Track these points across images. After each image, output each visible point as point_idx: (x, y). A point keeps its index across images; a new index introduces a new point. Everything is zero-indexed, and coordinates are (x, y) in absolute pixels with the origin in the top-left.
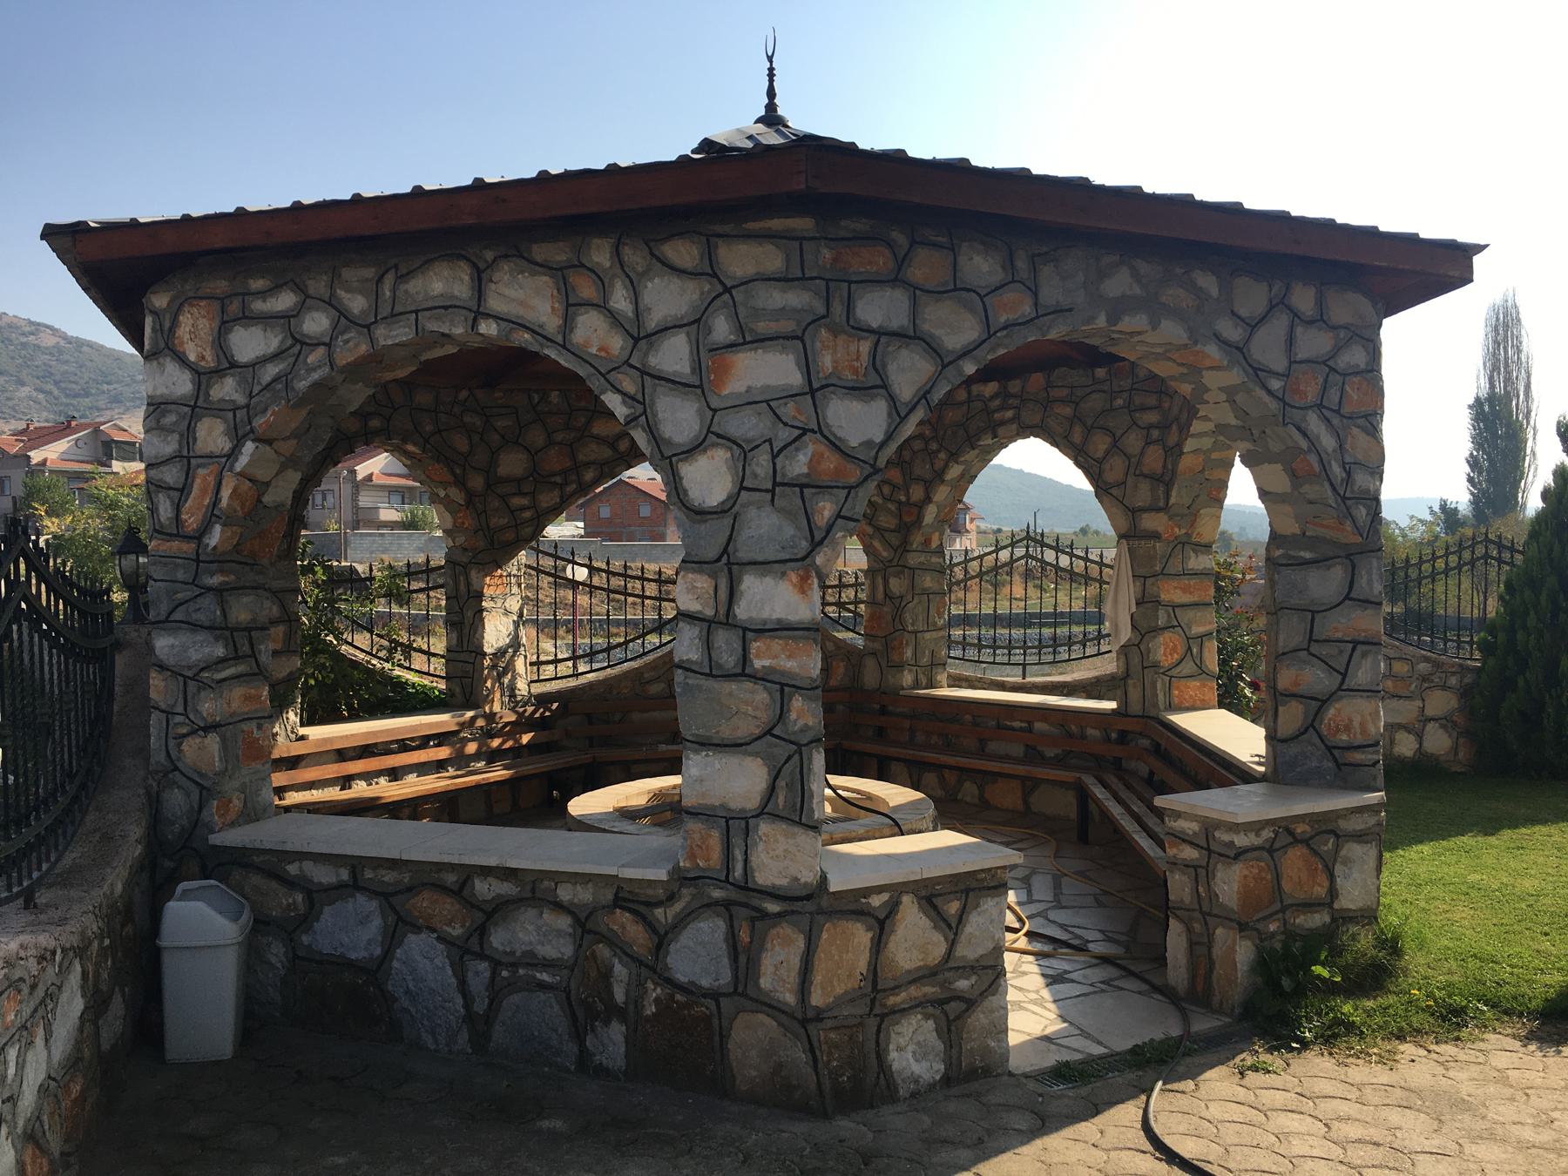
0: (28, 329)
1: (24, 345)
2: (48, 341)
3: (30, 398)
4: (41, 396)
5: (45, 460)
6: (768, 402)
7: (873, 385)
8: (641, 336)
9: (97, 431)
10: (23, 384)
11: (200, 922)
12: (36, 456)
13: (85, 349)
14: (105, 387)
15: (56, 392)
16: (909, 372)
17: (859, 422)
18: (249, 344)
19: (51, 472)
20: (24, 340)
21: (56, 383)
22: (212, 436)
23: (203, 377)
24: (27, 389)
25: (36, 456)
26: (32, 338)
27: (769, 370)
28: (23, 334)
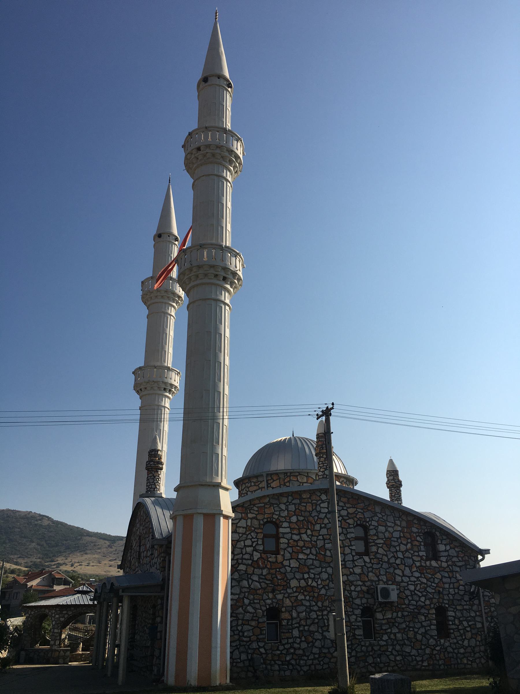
0: (39, 518)
1: (36, 525)
2: (46, 523)
3: (35, 548)
4: (39, 547)
5: (32, 586)
6: (57, 618)
7: (63, 617)
8: (52, 614)
9: (51, 574)
10: (33, 542)
11: (23, 653)
12: (29, 584)
13: (60, 525)
14: (65, 542)
15: (45, 545)
16: (66, 616)
17: (62, 619)
18: (32, 613)
19: (34, 590)
20: (36, 523)
21: (46, 541)
22: (29, 619)
23: (30, 615)
24: (34, 544)
25: (29, 584)
26: (40, 522)
27: (57, 616)
28: (37, 520)
